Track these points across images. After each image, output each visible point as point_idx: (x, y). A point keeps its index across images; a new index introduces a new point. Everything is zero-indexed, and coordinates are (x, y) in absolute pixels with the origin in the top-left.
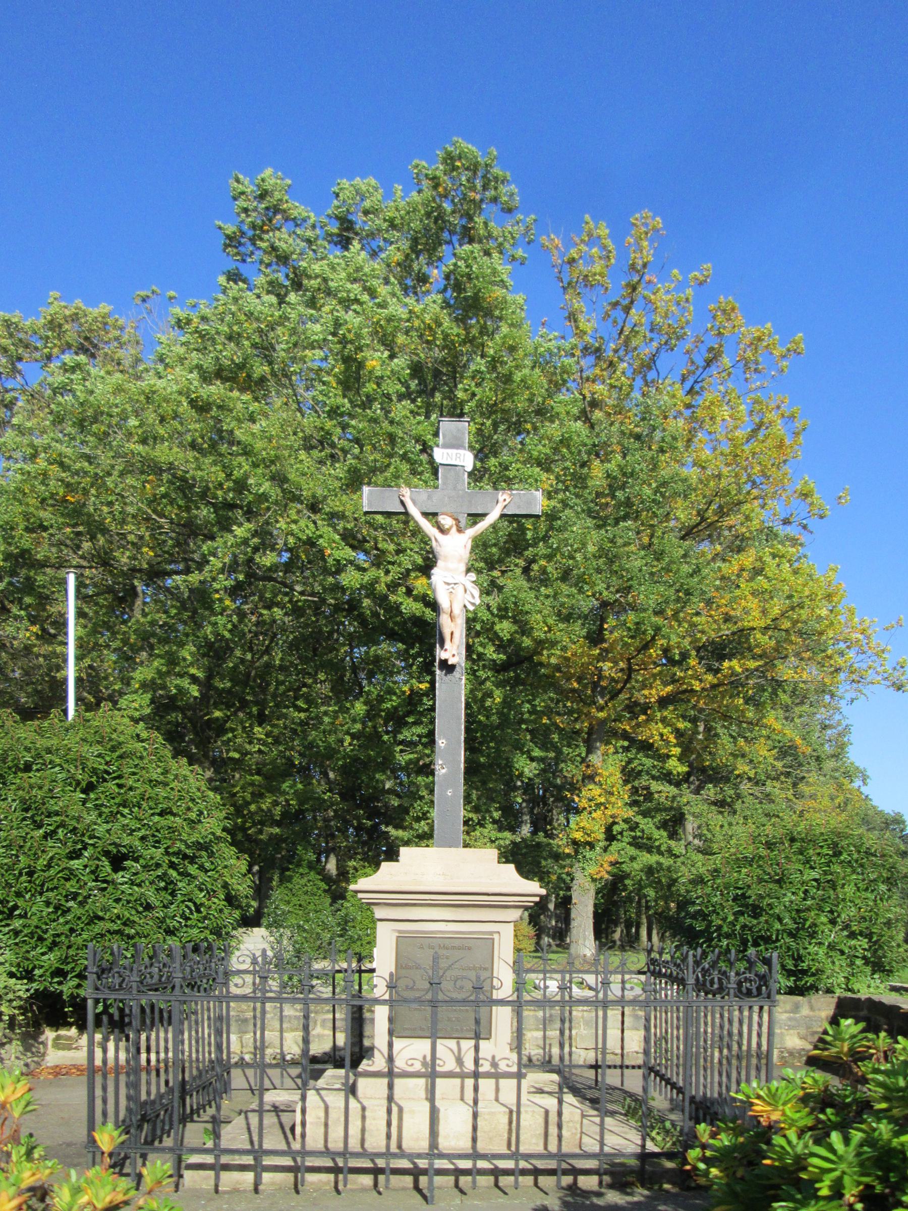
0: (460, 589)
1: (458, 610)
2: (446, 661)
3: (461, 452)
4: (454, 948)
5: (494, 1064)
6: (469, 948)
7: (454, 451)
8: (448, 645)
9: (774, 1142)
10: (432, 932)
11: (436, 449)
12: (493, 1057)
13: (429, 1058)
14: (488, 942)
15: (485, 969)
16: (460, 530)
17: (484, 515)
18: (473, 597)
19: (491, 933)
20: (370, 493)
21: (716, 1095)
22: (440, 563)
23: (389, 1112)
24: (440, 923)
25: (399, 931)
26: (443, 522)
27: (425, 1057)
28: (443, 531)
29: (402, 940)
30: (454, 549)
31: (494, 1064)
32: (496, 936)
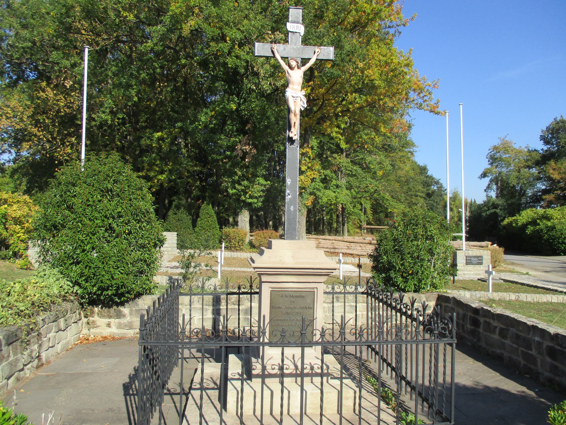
0: (299, 99)
1: (298, 112)
2: (292, 138)
3: (299, 25)
4: (296, 296)
5: (312, 368)
6: (303, 297)
7: (296, 25)
8: (293, 129)
9: (332, 49)
10: (287, 288)
11: (288, 23)
12: (310, 363)
13: (281, 364)
14: (312, 294)
15: (311, 308)
16: (298, 68)
17: (309, 59)
18: (304, 103)
19: (313, 288)
20: (258, 46)
21: (427, 383)
22: (290, 86)
23: (282, 392)
24: (291, 283)
25: (272, 288)
26: (292, 63)
27: (279, 364)
28: (291, 68)
29: (273, 293)
30: (296, 76)
31: (312, 368)
32: (315, 290)
